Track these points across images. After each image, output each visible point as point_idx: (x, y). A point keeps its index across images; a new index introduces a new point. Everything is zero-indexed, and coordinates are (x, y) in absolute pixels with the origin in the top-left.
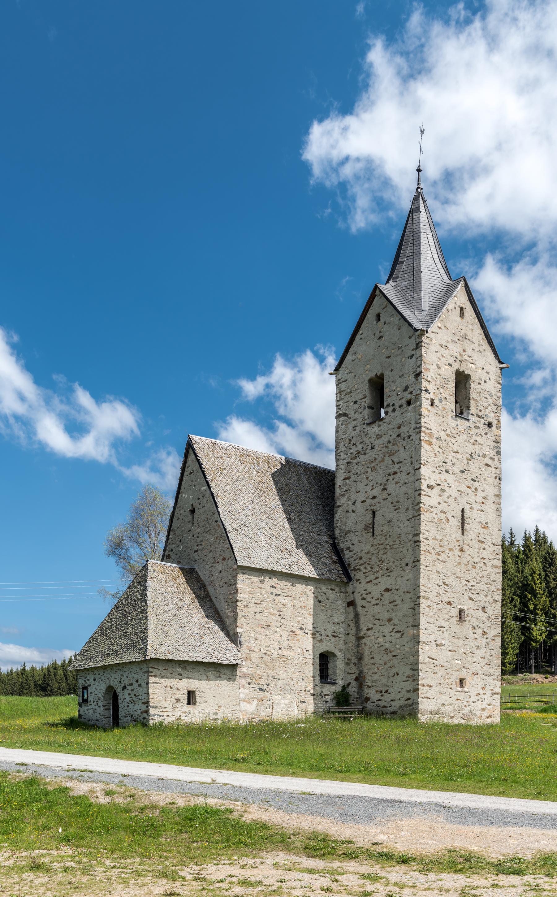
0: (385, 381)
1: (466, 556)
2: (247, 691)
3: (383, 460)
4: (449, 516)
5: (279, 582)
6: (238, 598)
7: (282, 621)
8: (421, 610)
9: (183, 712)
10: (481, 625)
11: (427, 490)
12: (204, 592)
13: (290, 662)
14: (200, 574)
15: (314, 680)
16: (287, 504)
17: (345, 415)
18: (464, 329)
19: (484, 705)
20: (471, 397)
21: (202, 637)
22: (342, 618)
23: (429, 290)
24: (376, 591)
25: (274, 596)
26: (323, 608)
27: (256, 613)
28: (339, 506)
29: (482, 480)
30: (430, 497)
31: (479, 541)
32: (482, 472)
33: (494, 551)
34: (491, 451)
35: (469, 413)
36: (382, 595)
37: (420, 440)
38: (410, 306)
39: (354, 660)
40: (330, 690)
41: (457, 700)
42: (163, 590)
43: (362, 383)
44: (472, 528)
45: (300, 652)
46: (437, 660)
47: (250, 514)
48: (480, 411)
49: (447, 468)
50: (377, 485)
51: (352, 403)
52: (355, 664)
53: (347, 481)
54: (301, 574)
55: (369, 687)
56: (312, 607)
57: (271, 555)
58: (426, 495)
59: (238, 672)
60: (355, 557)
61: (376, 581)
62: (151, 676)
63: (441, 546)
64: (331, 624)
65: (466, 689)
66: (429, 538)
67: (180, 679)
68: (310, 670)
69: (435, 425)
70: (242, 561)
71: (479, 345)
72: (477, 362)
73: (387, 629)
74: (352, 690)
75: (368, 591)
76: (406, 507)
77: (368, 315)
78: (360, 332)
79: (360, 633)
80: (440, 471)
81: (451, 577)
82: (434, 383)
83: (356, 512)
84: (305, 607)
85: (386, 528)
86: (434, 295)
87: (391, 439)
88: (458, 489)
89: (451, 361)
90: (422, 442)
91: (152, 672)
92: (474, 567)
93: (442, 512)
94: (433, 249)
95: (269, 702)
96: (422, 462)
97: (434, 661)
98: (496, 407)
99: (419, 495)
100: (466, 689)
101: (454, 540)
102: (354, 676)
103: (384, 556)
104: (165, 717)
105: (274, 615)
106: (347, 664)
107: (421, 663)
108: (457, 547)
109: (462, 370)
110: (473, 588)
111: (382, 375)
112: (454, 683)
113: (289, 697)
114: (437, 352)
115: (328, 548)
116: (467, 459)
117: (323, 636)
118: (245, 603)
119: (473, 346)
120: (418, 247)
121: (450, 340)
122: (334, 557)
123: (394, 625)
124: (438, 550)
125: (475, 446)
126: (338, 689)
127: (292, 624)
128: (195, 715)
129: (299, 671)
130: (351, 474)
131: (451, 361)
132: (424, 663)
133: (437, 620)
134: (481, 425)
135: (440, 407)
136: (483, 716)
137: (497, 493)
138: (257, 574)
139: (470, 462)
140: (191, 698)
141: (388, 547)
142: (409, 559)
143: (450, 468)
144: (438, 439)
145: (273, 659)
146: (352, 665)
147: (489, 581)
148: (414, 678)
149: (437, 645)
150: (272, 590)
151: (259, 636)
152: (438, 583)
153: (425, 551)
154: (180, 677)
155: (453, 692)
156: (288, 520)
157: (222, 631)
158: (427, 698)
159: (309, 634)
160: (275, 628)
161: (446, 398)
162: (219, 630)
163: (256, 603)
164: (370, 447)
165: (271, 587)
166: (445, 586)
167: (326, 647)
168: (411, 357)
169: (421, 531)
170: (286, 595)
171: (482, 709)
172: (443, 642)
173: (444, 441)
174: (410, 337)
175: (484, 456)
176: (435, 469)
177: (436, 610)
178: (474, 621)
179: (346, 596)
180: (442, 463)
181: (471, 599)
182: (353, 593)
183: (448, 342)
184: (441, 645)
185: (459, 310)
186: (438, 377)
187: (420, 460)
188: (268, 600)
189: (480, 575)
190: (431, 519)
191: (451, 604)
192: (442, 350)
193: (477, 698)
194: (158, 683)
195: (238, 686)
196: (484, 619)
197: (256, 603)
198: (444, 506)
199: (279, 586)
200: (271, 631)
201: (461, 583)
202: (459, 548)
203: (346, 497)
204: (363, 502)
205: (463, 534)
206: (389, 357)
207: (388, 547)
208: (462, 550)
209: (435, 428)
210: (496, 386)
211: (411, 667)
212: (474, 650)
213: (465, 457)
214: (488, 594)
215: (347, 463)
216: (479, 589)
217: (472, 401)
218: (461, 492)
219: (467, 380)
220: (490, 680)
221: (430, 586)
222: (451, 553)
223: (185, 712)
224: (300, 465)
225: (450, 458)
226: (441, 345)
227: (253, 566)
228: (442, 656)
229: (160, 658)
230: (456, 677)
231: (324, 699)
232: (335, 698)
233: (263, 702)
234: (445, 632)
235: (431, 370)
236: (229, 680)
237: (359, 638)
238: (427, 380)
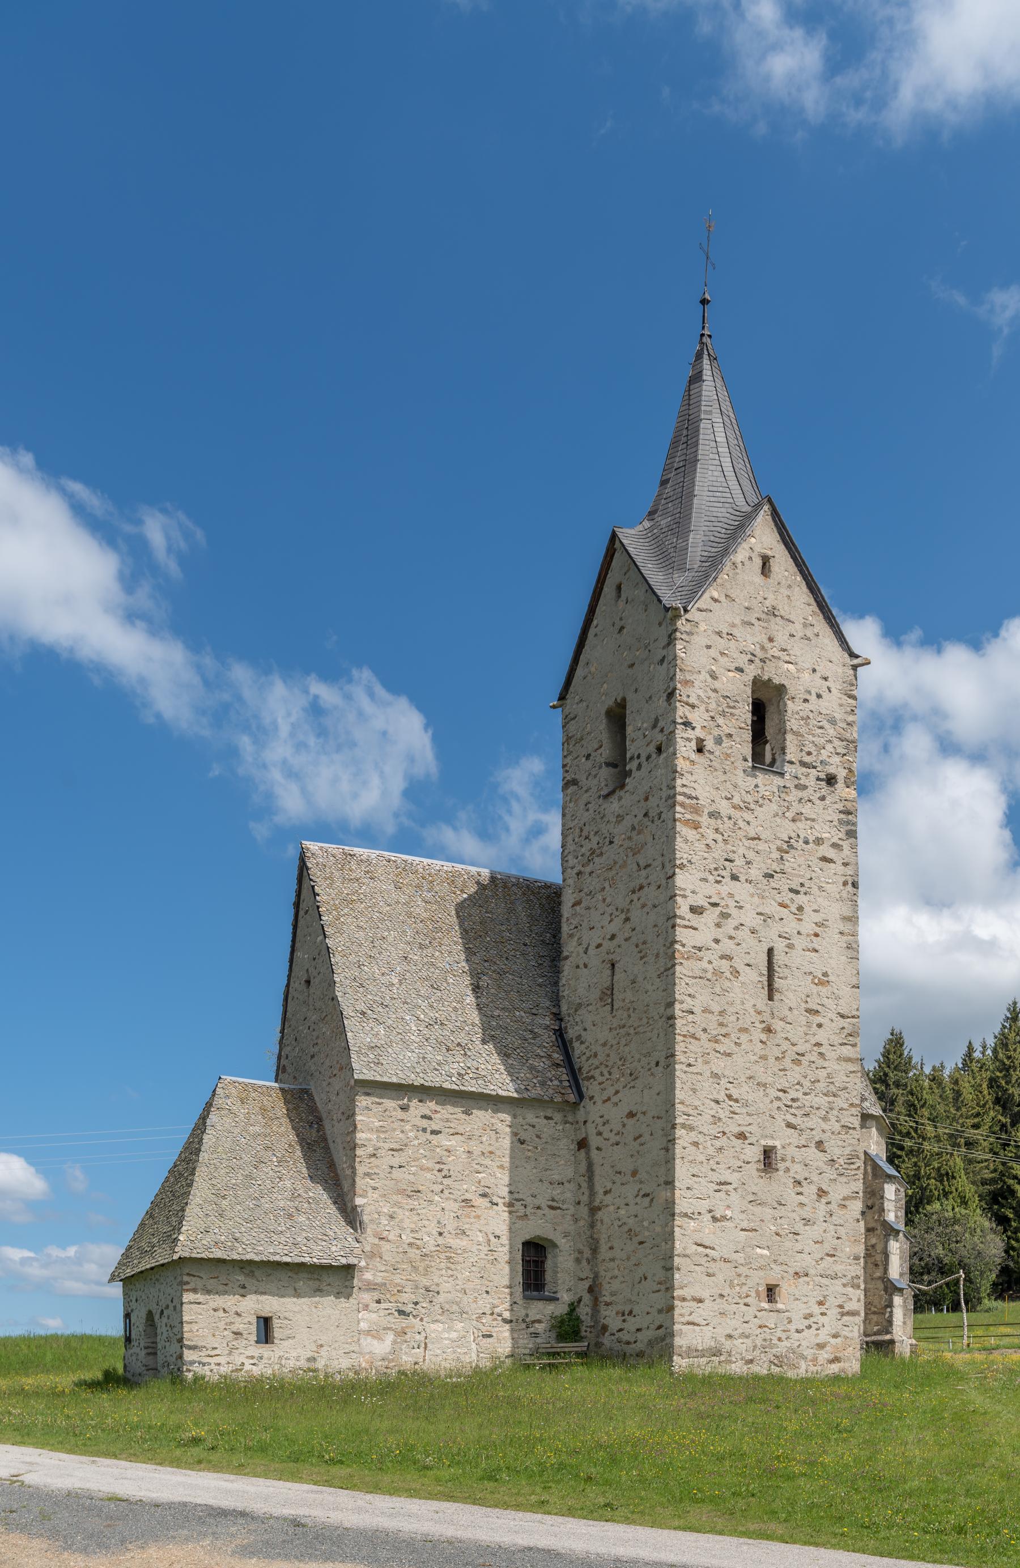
0: (627, 712)
1: (777, 1041)
2: (374, 1316)
3: (624, 865)
4: (739, 964)
5: (439, 1108)
6: (357, 1141)
7: (446, 1181)
8: (677, 1151)
9: (247, 1357)
10: (815, 1178)
11: (689, 915)
12: (318, 1131)
13: (461, 1260)
14: (316, 1098)
15: (511, 1294)
16: (476, 959)
17: (574, 782)
18: (771, 596)
19: (823, 1336)
20: (788, 728)
21: (290, 1216)
22: (570, 1173)
23: (704, 528)
24: (616, 1115)
25: (428, 1135)
26: (530, 1154)
27: (392, 1167)
28: (567, 958)
29: (815, 890)
30: (695, 929)
31: (809, 1011)
32: (813, 875)
33: (843, 1028)
34: (834, 831)
35: (784, 760)
36: (624, 1126)
37: (675, 820)
38: (667, 563)
39: (587, 1253)
40: (543, 1311)
41: (760, 1327)
42: (237, 1131)
43: (597, 718)
44: (793, 987)
45: (481, 1239)
46: (713, 1249)
47: (395, 981)
48: (809, 753)
49: (734, 871)
50: (618, 913)
51: (584, 759)
52: (588, 1261)
53: (578, 908)
54: (480, 1090)
55: (607, 1304)
56: (508, 1152)
57: (424, 1058)
58: (686, 927)
59: (356, 1282)
60: (588, 1054)
61: (615, 1099)
62: (187, 1290)
63: (721, 1024)
64: (546, 1184)
65: (780, 1306)
66: (695, 1010)
67: (243, 1296)
68: (502, 1272)
69: (707, 788)
70: (364, 1071)
71: (805, 625)
72: (799, 660)
73: (630, 1191)
74: (584, 1311)
75: (606, 1117)
76: (655, 952)
77: (605, 589)
78: (595, 622)
79: (594, 1201)
80: (719, 878)
81: (744, 1084)
82: (702, 708)
83: (589, 966)
84: (491, 1153)
85: (629, 995)
86: (712, 538)
87: (636, 821)
88: (759, 910)
89: (742, 661)
90: (678, 823)
91: (188, 1283)
92: (797, 1062)
93: (722, 957)
94: (723, 450)
95: (417, 1337)
96: (678, 862)
97: (708, 1251)
98: (845, 743)
99: (674, 926)
100: (780, 1306)
101: (752, 1011)
102: (586, 1284)
103: (627, 1049)
104: (213, 1366)
105: (429, 1170)
106: (578, 1261)
107: (678, 1255)
108: (757, 1024)
109: (766, 678)
110: (794, 1105)
111: (624, 699)
112: (753, 1294)
113: (459, 1326)
114: (709, 647)
115: (548, 1038)
116: (779, 849)
117: (528, 1208)
118: (370, 1150)
119: (791, 629)
120: (694, 450)
121: (737, 621)
122: (556, 1055)
123: (641, 1182)
124: (715, 1032)
125: (798, 824)
126: (560, 1309)
127: (465, 1187)
128: (286, 1357)
129: (479, 1275)
130: (582, 894)
131: (742, 661)
132: (685, 1256)
133: (712, 1170)
134: (811, 782)
135: (717, 753)
136: (820, 1358)
137: (848, 913)
138: (394, 1093)
139: (786, 856)
141: (632, 1031)
142: (660, 1055)
143: (742, 870)
144: (714, 815)
145: (426, 1255)
146: (584, 1263)
147: (832, 1088)
148: (668, 1286)
149: (715, 1219)
150: (425, 1123)
151: (400, 1211)
152: (715, 1096)
153: (684, 1036)
154: (242, 1291)
155: (751, 1311)
156: (473, 990)
157: (335, 1203)
158: (693, 1324)
159: (501, 1205)
160: (430, 1195)
161: (730, 735)
162: (329, 1202)
163: (392, 1150)
164: (607, 840)
165: (423, 1117)
167: (536, 1228)
168: (662, 661)
169: (677, 996)
170: (452, 1131)
171: (818, 1345)
172: (729, 1213)
173: (726, 819)
174: (660, 624)
175: (819, 841)
176: (707, 875)
177: (711, 1151)
178: (799, 1170)
179: (576, 1130)
180: (722, 862)
181: (789, 1125)
182: (585, 1122)
183: (733, 625)
184: (724, 1218)
185: (758, 562)
186: (713, 695)
187: (675, 859)
188: (416, 1142)
189: (811, 1077)
190: (698, 973)
191: (746, 1138)
192: (721, 643)
193: (807, 1322)
194: (199, 1303)
195: (355, 1307)
196: (821, 1164)
197: (392, 1150)
198: (727, 946)
199: (438, 1116)
200: (421, 1201)
201: (766, 1095)
202: (764, 1025)
203: (576, 939)
204: (599, 946)
205: (771, 998)
206: (632, 665)
207: (632, 1031)
208: (769, 1030)
209: (707, 794)
210: (844, 702)
211: (662, 1263)
212: (799, 1227)
213: (774, 847)
214: (830, 1116)
215: (578, 874)
216: (807, 1104)
217: (789, 737)
218: (766, 917)
219: (781, 695)
220: (836, 1287)
221: (697, 1103)
222: (744, 1038)
223: (252, 1357)
224: (517, 885)
225: (741, 851)
226: (719, 634)
227: (385, 1079)
228: (725, 1240)
229: (199, 1256)
230: (759, 1280)
231: (532, 1330)
232: (553, 1327)
233: (407, 1337)
234: (733, 1193)
235: (697, 683)
236: (338, 1295)
237: (593, 1210)
238: (687, 704)
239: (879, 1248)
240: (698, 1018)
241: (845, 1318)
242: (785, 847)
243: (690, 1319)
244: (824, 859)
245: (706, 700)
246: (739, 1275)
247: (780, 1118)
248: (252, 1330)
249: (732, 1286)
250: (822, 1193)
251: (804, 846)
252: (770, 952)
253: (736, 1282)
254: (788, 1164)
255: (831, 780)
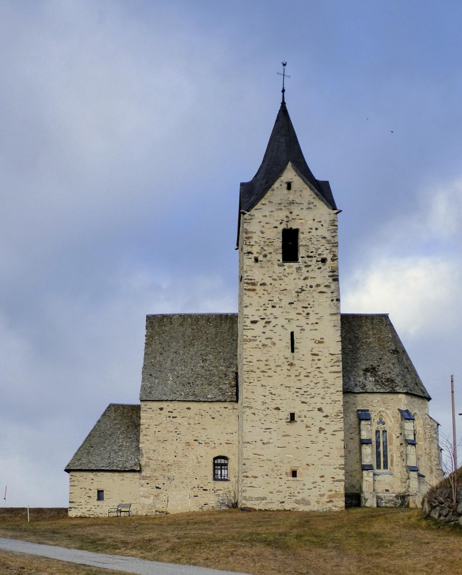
2: (146, 489)
33: (332, 359)
41: (288, 487)
48: (312, 252)
66: (253, 361)
93: (267, 339)
110: (305, 394)
116: (297, 292)
127: (187, 437)
131: (277, 224)
140: (100, 495)
147: (326, 385)
149: (264, 444)
150: (170, 414)
152: (264, 394)
155: (282, 482)
158: (253, 487)
161: (271, 253)
166: (272, 396)
172: (271, 441)
175: (318, 285)
176: (260, 308)
181: (303, 402)
184: (268, 443)
188: (166, 422)
193: (314, 485)
205: (293, 351)
210: (330, 229)
212: (309, 444)
223: (95, 506)
231: (216, 493)
239: (404, 453)
240: (255, 363)
241: (335, 483)
242: (300, 290)
243: (251, 485)
244: (321, 292)
245: (259, 242)
246: (277, 466)
247: (298, 399)
248: (95, 495)
249: (273, 470)
250: (321, 429)
251: (310, 289)
252: (292, 334)
253: (275, 469)
254: (303, 418)
255: (324, 261)
